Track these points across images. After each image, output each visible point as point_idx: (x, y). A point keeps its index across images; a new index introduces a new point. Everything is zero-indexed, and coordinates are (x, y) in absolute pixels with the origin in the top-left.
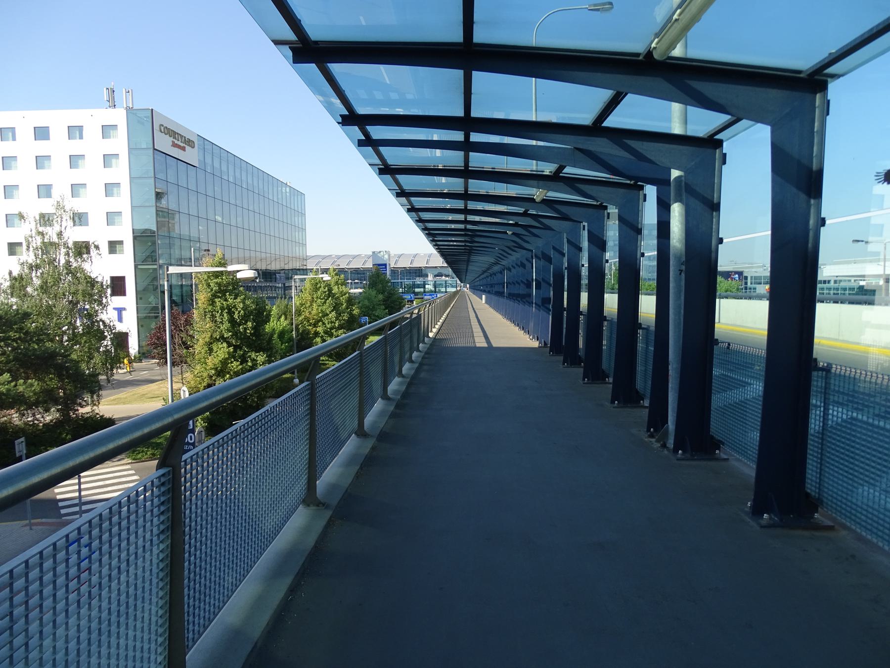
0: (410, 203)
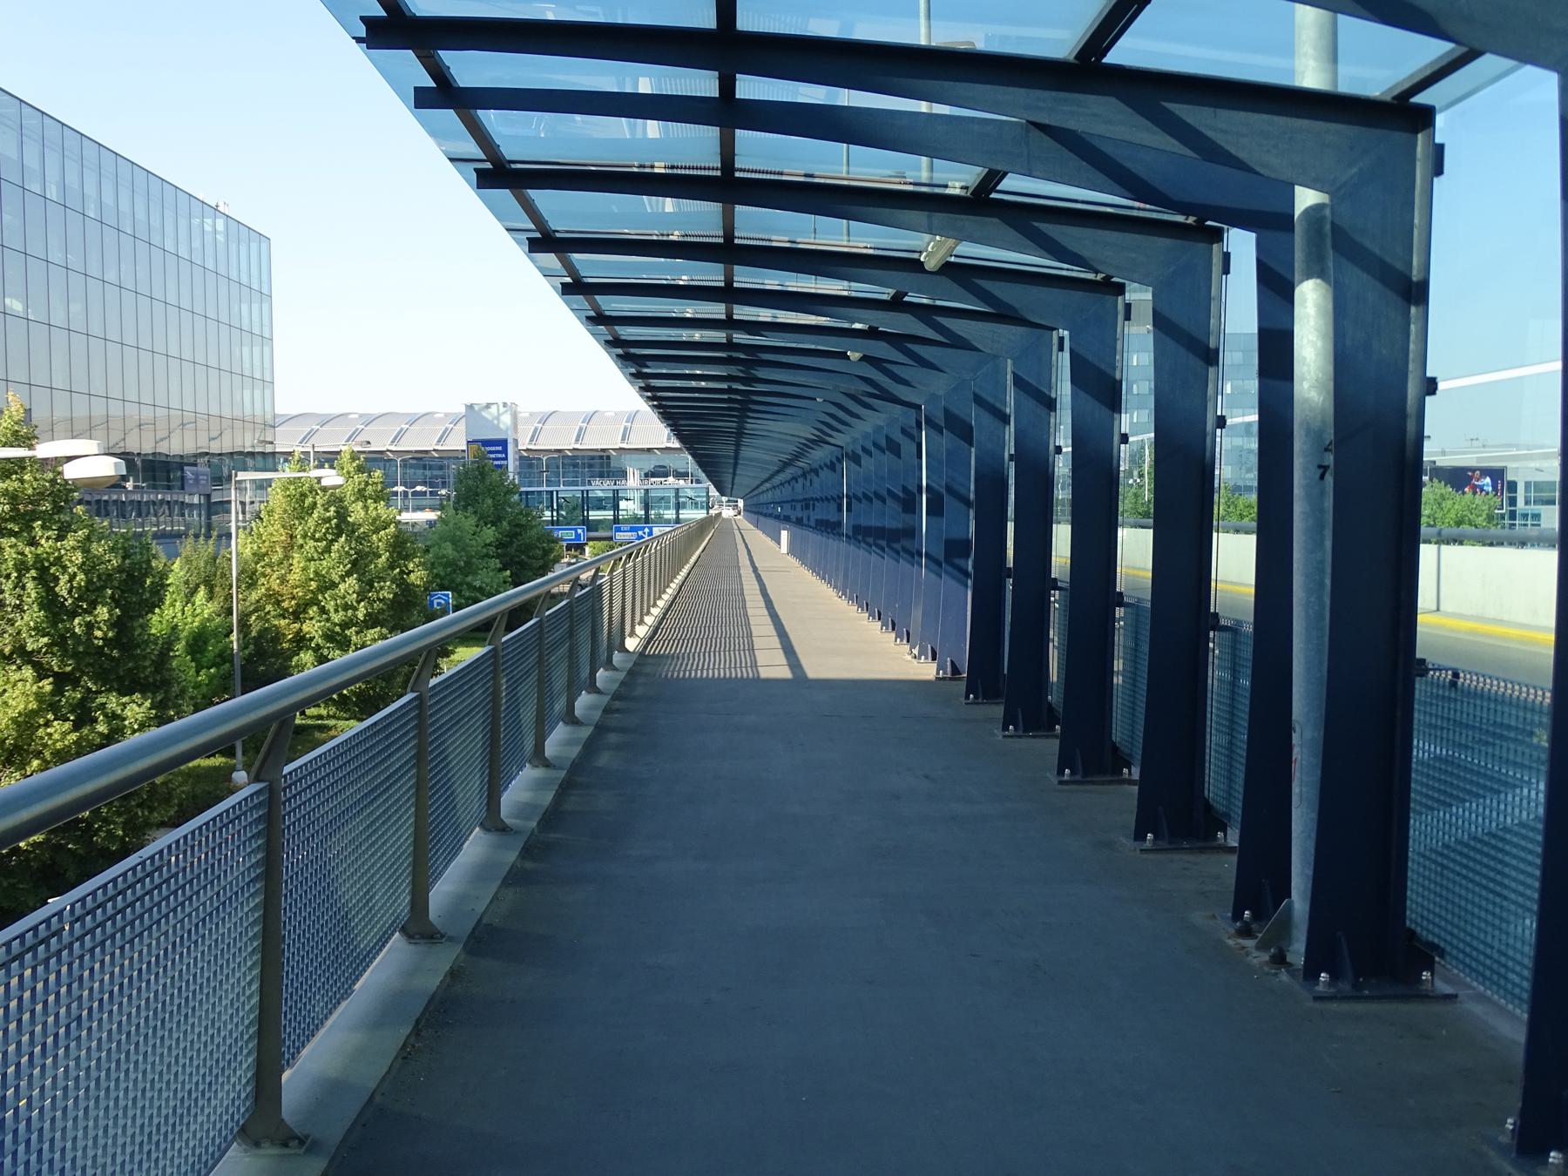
0: (570, 268)
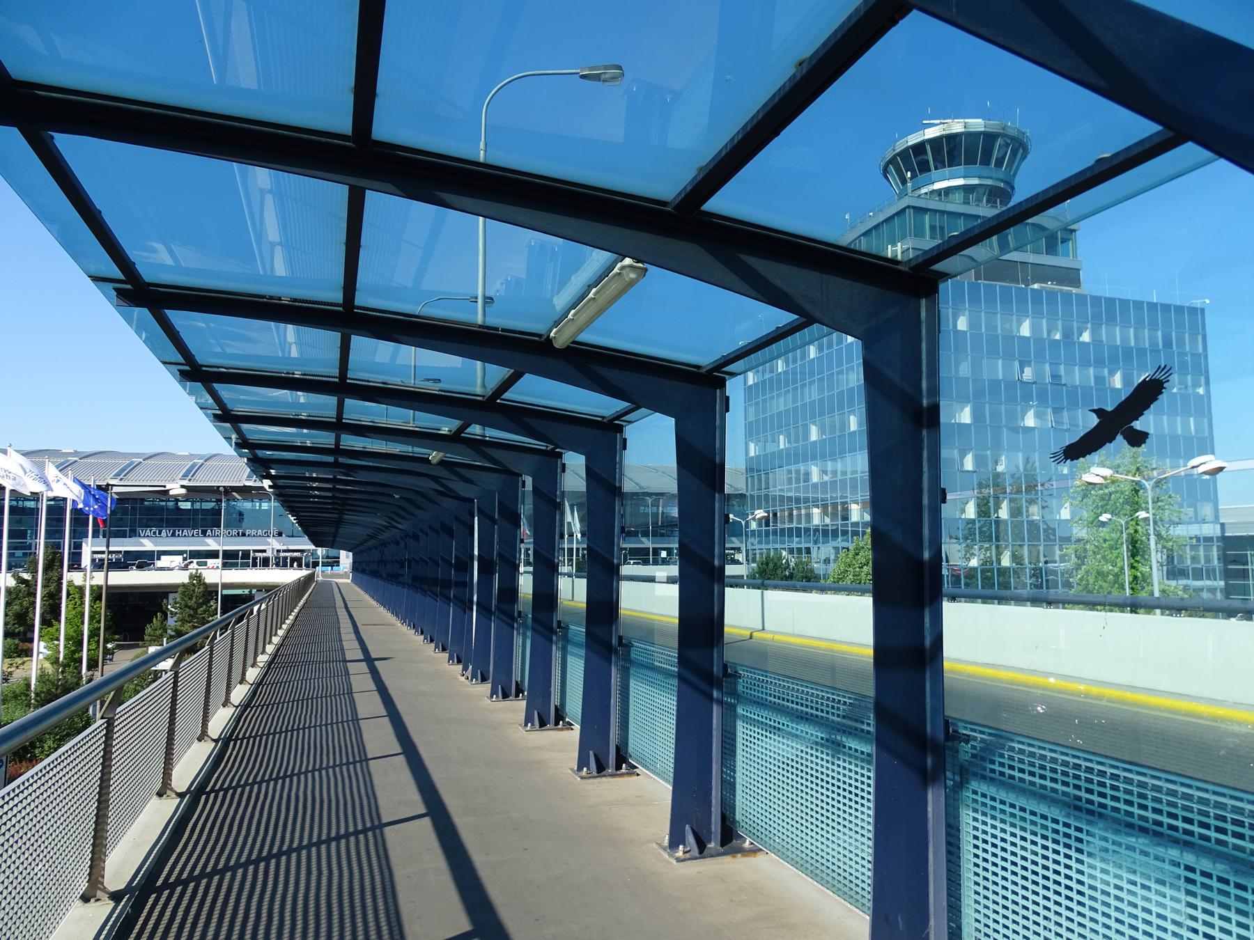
0: (240, 433)
